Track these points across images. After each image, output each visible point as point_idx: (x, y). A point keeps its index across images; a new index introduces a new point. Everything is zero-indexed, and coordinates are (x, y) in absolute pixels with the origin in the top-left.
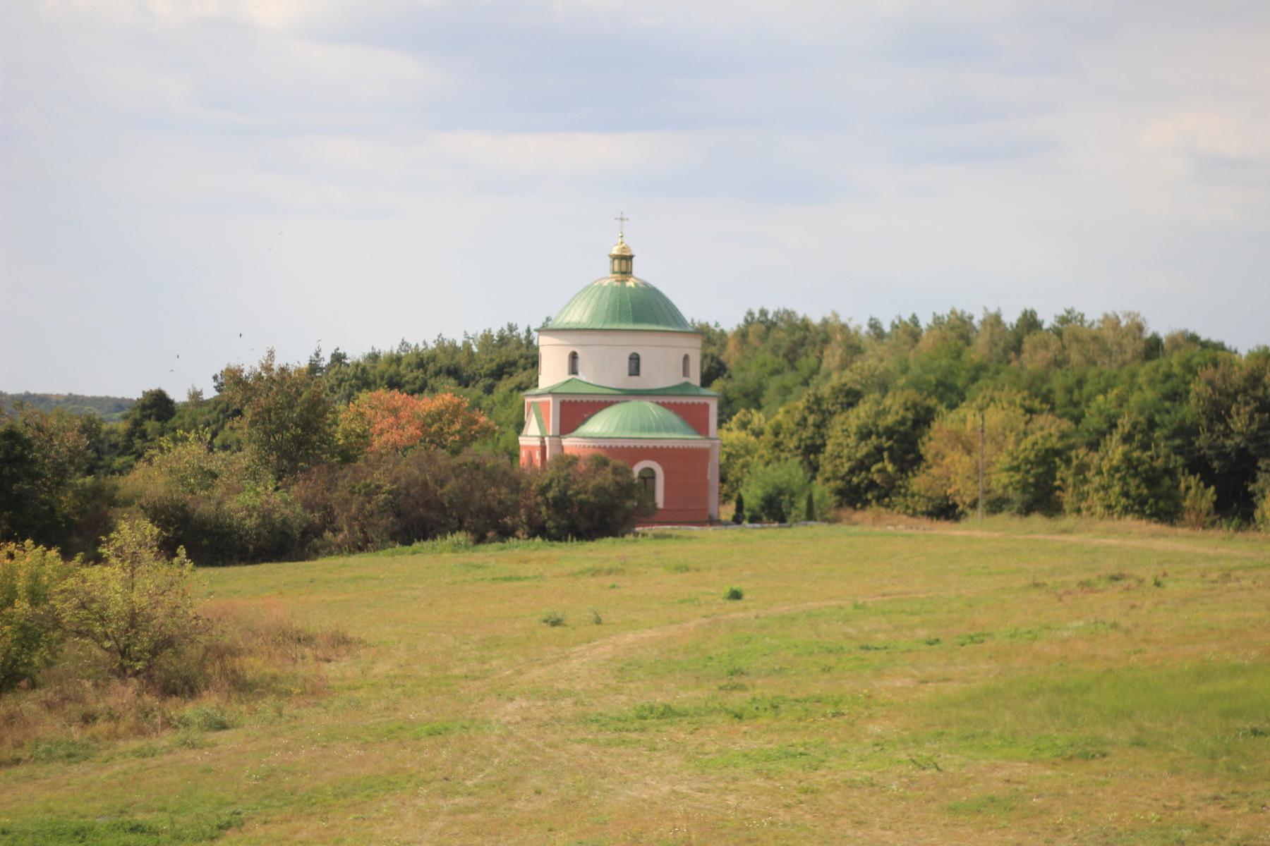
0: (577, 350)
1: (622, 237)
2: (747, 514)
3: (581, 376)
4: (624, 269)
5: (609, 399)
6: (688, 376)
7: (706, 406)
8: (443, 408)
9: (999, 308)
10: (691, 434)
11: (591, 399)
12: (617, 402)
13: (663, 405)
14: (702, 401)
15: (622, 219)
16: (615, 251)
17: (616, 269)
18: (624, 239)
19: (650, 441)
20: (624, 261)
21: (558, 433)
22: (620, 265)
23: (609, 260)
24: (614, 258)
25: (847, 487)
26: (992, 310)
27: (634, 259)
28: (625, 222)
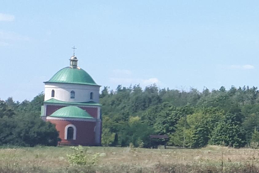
0: (54, 89)
1: (74, 54)
2: (120, 142)
3: (55, 98)
4: (74, 64)
5: (63, 105)
6: (92, 99)
7: (96, 109)
8: (149, 100)
9: (165, 88)
10: (90, 117)
11: (57, 105)
12: (66, 106)
13: (78, 107)
14: (95, 107)
15: (74, 48)
16: (72, 58)
17: (71, 64)
18: (75, 54)
19: (72, 119)
20: (75, 61)
21: (45, 115)
22: (73, 63)
23: (69, 61)
24: (71, 60)
25: (171, 132)
26: (11, 97)
27: (78, 62)
28: (75, 49)
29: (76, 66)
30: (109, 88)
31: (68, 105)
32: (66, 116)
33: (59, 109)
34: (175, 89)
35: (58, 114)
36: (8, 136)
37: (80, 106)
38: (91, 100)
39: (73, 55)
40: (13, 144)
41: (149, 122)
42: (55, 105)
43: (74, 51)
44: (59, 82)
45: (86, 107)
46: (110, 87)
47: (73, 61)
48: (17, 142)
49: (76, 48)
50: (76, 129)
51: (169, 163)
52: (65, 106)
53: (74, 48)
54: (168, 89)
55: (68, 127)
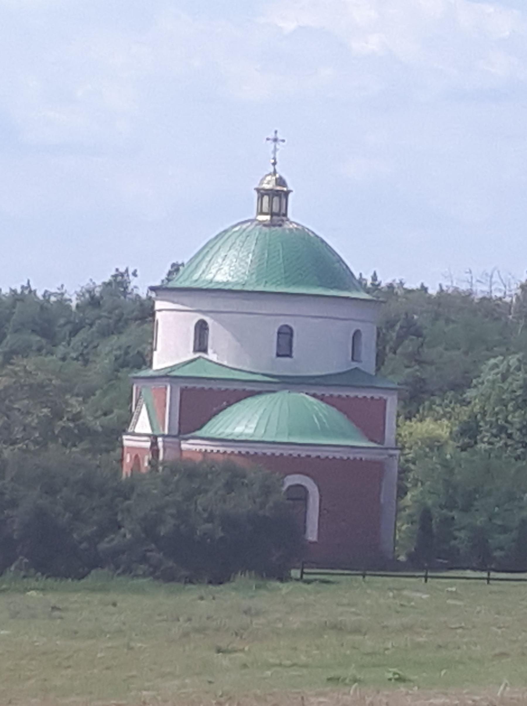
5: (257, 389)
11: (223, 387)
15: (275, 140)
16: (269, 184)
23: (255, 195)
24: (262, 193)
27: (291, 196)
29: (285, 215)
30: (135, 274)
31: (267, 387)
32: (252, 435)
33: (238, 400)
34: (464, 287)
35: (213, 431)
36: (101, 534)
37: (327, 392)
38: (355, 365)
39: (271, 170)
40: (128, 571)
41: (506, 445)
42: (215, 386)
43: (275, 150)
44: (210, 286)
45: (203, 389)
46: (138, 273)
47: (272, 193)
48: (144, 559)
49: (283, 141)
50: (317, 494)
51: (360, 678)
52: (252, 394)
53: (275, 140)
54: (374, 277)
55: (299, 482)
